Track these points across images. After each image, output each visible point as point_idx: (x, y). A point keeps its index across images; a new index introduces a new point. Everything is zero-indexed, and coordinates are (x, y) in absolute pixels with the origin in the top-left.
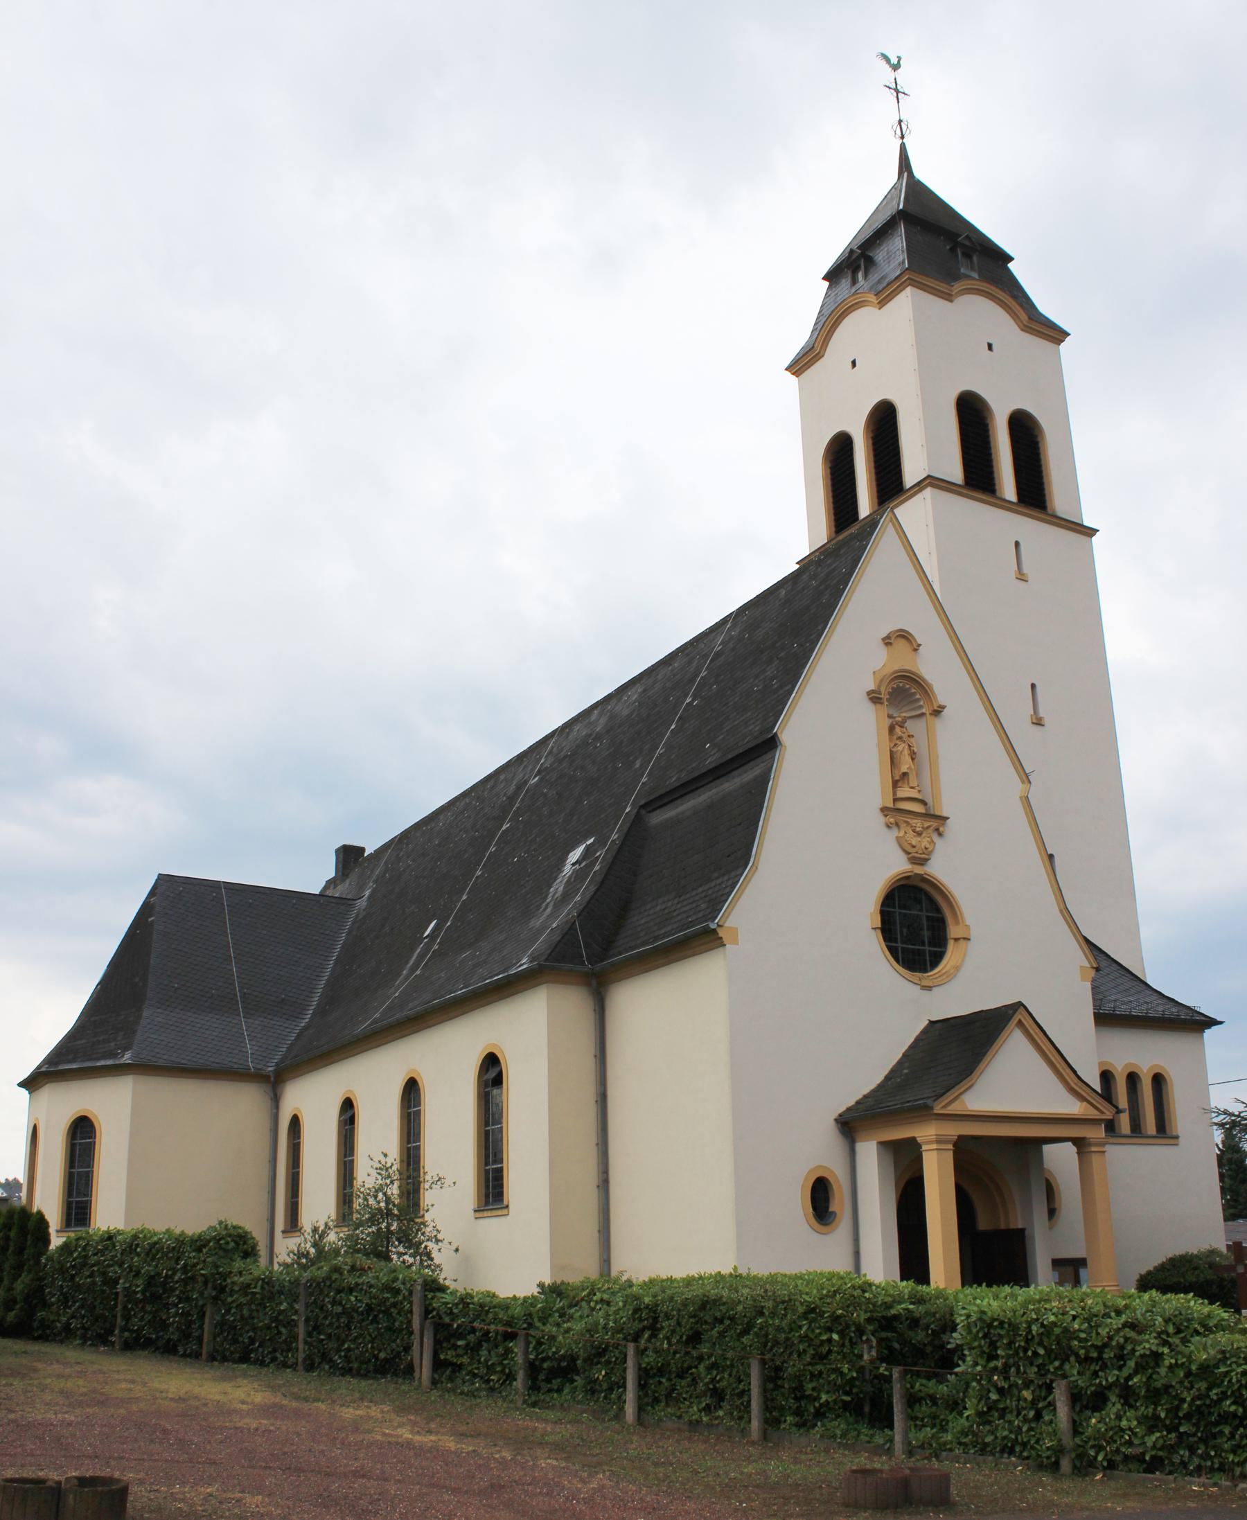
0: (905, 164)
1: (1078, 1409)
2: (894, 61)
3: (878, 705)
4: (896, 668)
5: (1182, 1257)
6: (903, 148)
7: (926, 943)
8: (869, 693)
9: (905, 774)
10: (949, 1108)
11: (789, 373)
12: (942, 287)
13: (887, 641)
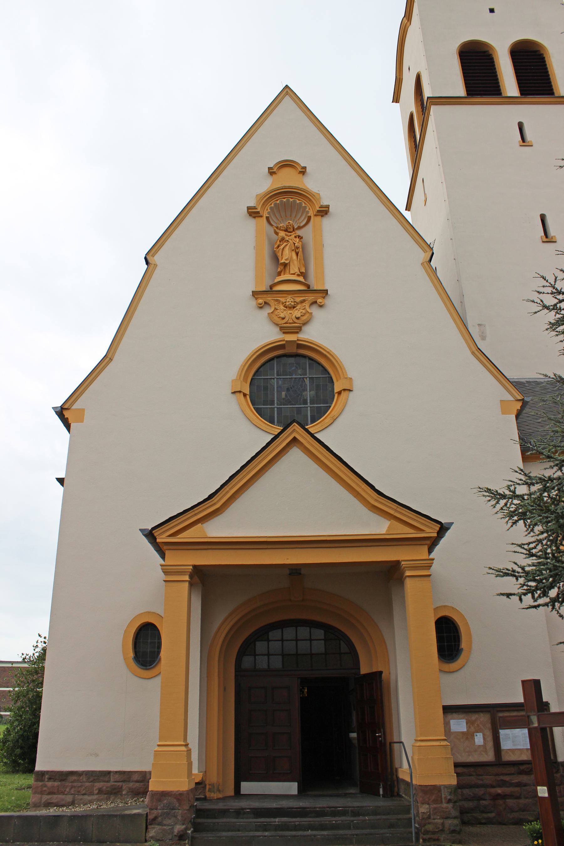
1: (530, 824)
7: (309, 401)
8: (249, 208)
10: (179, 536)
11: (407, 211)
13: (271, 172)
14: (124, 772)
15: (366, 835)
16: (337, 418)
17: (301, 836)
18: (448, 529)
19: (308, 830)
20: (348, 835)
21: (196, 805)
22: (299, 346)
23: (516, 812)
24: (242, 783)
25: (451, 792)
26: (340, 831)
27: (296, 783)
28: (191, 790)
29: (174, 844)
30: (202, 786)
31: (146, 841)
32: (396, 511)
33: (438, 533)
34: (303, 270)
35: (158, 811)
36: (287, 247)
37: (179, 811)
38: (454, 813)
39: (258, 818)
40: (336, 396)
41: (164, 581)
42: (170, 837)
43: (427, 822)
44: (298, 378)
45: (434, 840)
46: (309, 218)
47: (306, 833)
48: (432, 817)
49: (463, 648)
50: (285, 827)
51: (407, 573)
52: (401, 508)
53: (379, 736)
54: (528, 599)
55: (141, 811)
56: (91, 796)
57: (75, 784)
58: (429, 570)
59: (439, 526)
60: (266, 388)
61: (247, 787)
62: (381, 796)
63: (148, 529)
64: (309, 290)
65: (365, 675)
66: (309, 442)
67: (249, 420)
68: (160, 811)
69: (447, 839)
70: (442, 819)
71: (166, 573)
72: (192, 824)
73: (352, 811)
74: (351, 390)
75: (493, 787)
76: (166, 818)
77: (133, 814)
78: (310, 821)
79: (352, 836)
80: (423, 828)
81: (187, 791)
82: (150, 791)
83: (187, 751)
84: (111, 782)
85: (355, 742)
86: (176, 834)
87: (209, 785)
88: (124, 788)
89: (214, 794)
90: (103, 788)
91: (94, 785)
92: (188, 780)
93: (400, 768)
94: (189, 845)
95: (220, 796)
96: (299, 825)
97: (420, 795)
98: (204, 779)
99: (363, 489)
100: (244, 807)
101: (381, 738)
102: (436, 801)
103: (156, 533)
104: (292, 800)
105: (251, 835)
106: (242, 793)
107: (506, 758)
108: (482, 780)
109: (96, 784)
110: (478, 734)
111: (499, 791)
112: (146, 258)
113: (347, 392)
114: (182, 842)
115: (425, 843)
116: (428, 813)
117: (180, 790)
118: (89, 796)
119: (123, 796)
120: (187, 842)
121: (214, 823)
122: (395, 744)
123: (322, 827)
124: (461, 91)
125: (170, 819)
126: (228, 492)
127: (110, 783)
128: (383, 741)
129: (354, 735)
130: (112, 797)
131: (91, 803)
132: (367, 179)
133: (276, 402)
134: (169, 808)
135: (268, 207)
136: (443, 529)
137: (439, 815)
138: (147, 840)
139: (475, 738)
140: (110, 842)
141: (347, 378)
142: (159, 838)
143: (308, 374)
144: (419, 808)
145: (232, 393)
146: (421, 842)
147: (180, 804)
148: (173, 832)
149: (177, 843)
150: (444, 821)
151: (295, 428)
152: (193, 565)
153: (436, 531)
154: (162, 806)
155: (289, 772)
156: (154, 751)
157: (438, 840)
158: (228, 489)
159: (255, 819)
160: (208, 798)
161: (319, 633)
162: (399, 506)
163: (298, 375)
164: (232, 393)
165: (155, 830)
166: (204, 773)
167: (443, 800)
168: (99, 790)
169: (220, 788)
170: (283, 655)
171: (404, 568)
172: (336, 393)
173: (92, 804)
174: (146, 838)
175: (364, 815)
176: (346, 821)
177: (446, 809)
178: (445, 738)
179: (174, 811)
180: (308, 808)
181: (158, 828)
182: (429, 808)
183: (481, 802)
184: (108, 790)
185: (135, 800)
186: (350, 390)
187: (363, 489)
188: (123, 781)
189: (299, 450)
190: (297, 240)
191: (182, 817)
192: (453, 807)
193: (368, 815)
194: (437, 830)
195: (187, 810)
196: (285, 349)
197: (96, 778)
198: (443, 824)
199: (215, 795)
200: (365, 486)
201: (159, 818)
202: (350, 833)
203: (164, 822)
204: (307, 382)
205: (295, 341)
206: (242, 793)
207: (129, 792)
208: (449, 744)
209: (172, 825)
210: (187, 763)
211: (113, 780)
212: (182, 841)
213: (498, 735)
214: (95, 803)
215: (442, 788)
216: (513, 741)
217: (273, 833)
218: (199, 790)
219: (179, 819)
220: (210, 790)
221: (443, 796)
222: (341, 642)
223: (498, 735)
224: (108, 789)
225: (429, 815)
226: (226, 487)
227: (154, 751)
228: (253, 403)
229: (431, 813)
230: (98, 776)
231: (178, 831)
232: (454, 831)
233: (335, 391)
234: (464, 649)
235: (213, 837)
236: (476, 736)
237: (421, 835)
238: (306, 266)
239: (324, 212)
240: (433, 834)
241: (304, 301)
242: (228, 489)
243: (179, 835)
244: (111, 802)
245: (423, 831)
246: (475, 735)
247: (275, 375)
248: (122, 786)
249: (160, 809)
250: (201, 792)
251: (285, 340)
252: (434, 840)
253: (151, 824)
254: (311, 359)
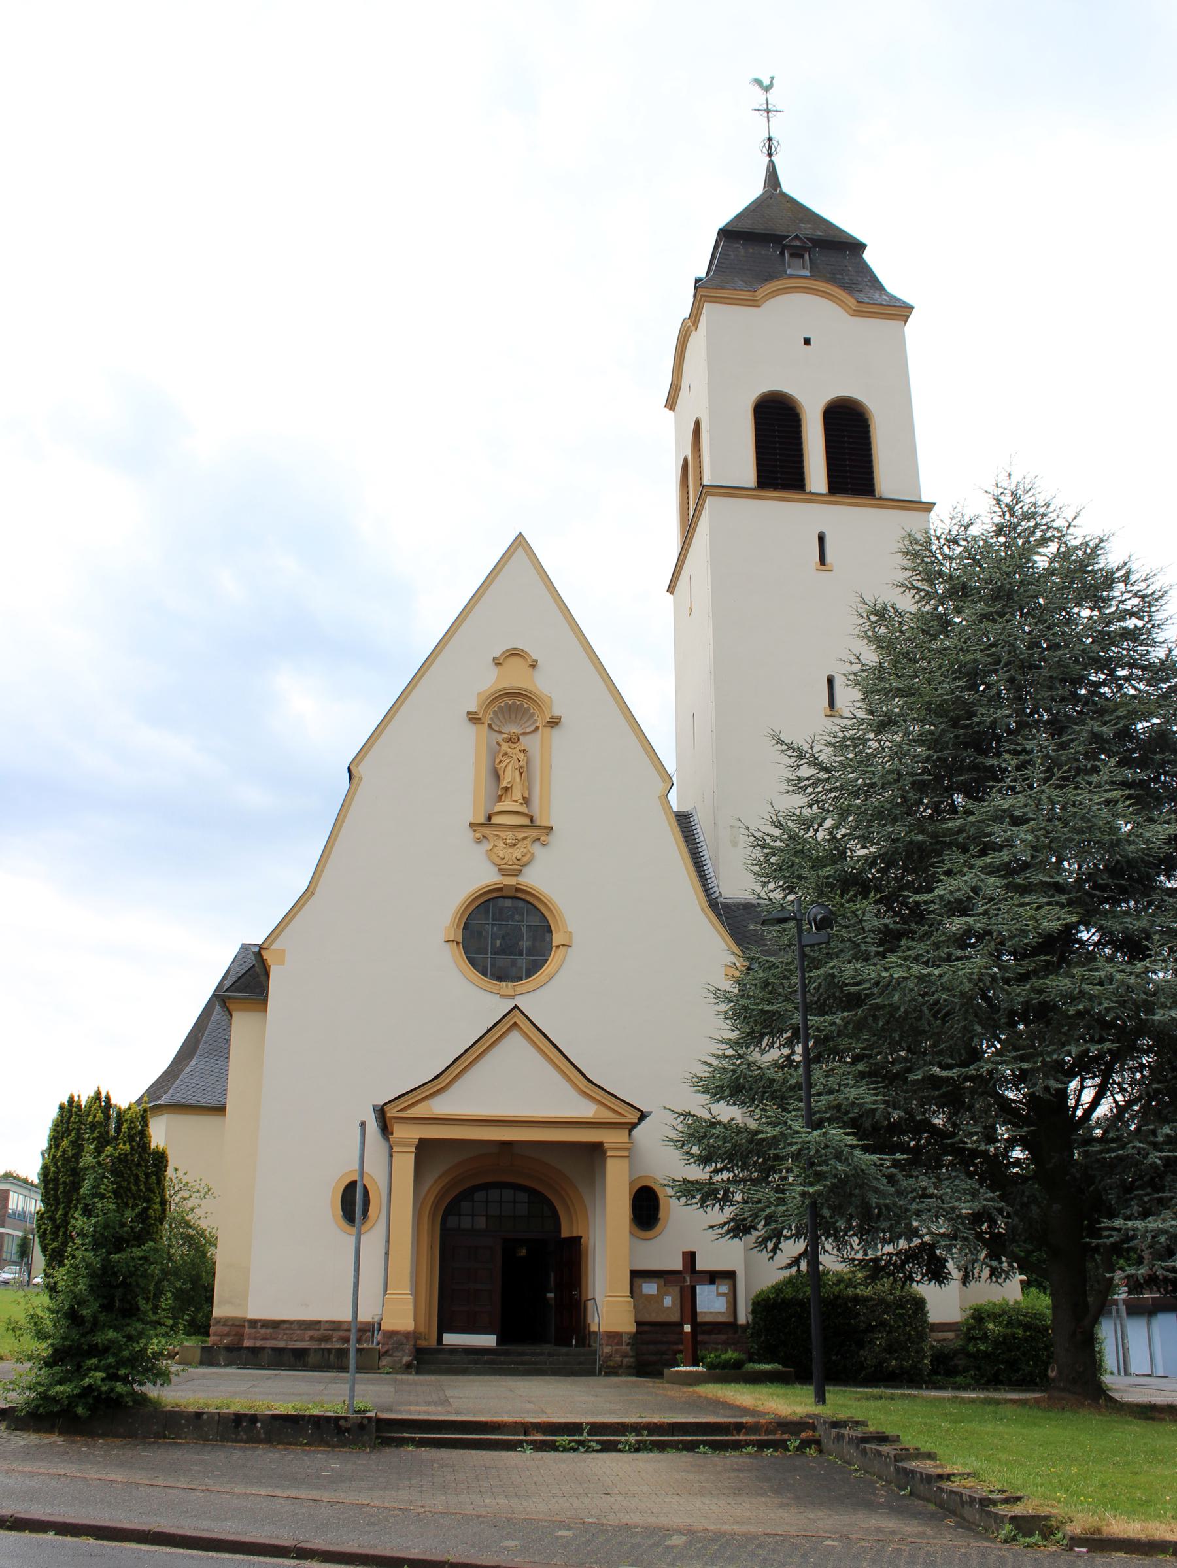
0: (772, 178)
2: (766, 82)
3: (477, 725)
4: (505, 685)
5: (56, 1139)
6: (772, 164)
8: (469, 713)
9: (507, 789)
12: (745, 295)
13: (497, 662)
22: (518, 890)
24: (563, 1236)
34: (526, 795)
36: (511, 764)
38: (631, 1354)
40: (554, 949)
46: (537, 728)
54: (683, 1199)
57: (288, 1332)
61: (450, 1339)
64: (532, 824)
85: (553, 1302)
102: (617, 1344)
103: (386, 1108)
112: (349, 769)
113: (566, 947)
124: (747, 475)
129: (551, 1295)
132: (607, 679)
135: (491, 710)
136: (643, 1116)
161: (523, 1197)
170: (487, 1216)
188: (334, 1330)
190: (522, 755)
198: (622, 1361)
204: (524, 929)
238: (530, 789)
239: (554, 723)
241: (526, 838)
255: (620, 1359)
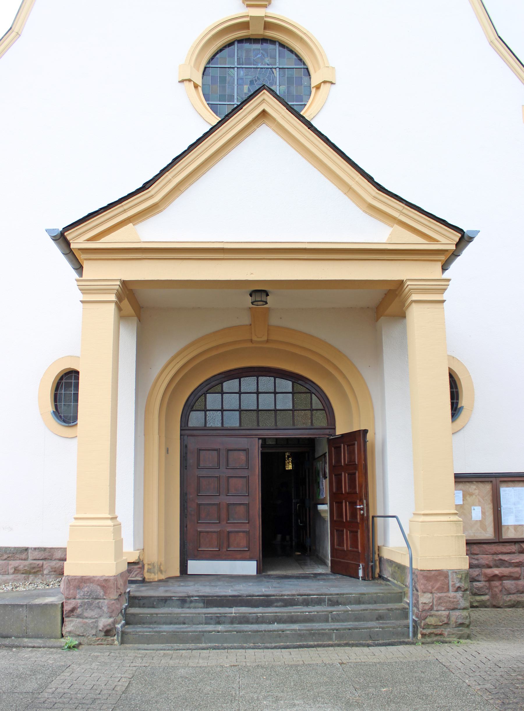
10: (103, 240)
14: (45, 549)
15: (350, 630)
16: (314, 117)
17: (265, 631)
18: (470, 239)
19: (274, 623)
20: (327, 631)
21: (129, 592)
22: (268, 26)
23: (514, 594)
24: (189, 562)
25: (461, 579)
26: (314, 624)
27: (255, 562)
28: (122, 574)
29: (100, 640)
30: (138, 566)
31: (62, 636)
32: (401, 213)
33: (457, 245)
35: (77, 600)
37: (105, 601)
39: (208, 608)
40: (313, 91)
41: (82, 302)
42: (94, 632)
43: (428, 614)
44: (265, 68)
45: (436, 635)
47: (271, 627)
48: (435, 608)
49: (463, 407)
50: (244, 620)
51: (413, 298)
52: (409, 208)
53: (361, 509)
55: (56, 600)
56: (6, 575)
58: (442, 295)
59: (460, 235)
60: (223, 80)
62: (361, 579)
63: (58, 229)
65: (343, 435)
66: (284, 116)
67: (201, 116)
68: (79, 601)
69: (453, 634)
70: (448, 610)
71: (84, 291)
72: (123, 616)
73: (329, 600)
74: (333, 82)
75: (490, 567)
76: (88, 610)
77: (44, 604)
78: (276, 613)
79: (332, 631)
80: (423, 622)
81: (115, 576)
82: (66, 576)
83: (114, 526)
84: (29, 560)
86: (101, 629)
87: (148, 564)
88: (45, 567)
89: (155, 575)
90: (20, 567)
91: (8, 564)
92: (115, 563)
93: (384, 546)
94: (118, 641)
95: (163, 577)
96: (263, 617)
97: (421, 582)
98: (141, 558)
99: (357, 183)
100: (191, 595)
101: (363, 510)
102: (441, 589)
103: (69, 235)
104: (251, 584)
105: (200, 630)
106: (189, 573)
107: (509, 534)
108: (477, 559)
109: (11, 562)
110: (476, 508)
111: (496, 571)
113: (328, 85)
114: (110, 639)
115: (425, 638)
116: (430, 603)
117: (105, 576)
118: (4, 575)
119: (45, 576)
120: (116, 637)
121: (152, 614)
122: (378, 518)
123: (292, 620)
125: (93, 610)
126: (170, 181)
127: (28, 561)
128: (365, 515)
130: (31, 577)
131: (6, 583)
133: (236, 97)
134: (91, 598)
137: (444, 606)
138: (64, 635)
139: (472, 512)
140: (15, 637)
141: (328, 67)
142: (79, 633)
143: (278, 64)
144: (419, 598)
145: (180, 82)
146: (419, 638)
147: (105, 593)
148: (97, 627)
149: (102, 639)
150: (449, 613)
151: (265, 97)
152: (121, 280)
153: (456, 243)
154: (82, 594)
155: (247, 549)
156: (70, 526)
157: (441, 634)
158: (170, 177)
159: (205, 609)
160: (147, 580)
161: (286, 385)
162: (406, 207)
163: (265, 65)
164: (180, 82)
165: (74, 623)
166: (142, 550)
167: (451, 588)
168: (15, 570)
169: (162, 568)
170: (240, 410)
171: (410, 289)
172: (313, 88)
173: (7, 585)
174: (63, 633)
175: (344, 604)
176: (323, 611)
177: (454, 598)
178: (456, 512)
179: (97, 601)
180: (274, 596)
181: (77, 622)
182: (432, 597)
183: (474, 583)
184: (26, 570)
185: (59, 581)
186: (332, 83)
187: (357, 183)
188: (45, 559)
189: (270, 129)
191: (108, 608)
192: (463, 597)
193: (350, 603)
194: (441, 624)
195: (115, 600)
196: (249, 30)
197: (10, 555)
198: (448, 617)
199: (156, 577)
200: (360, 177)
201: (78, 609)
202: (329, 627)
203: (86, 614)
204: (277, 73)
205: (262, 18)
206: (189, 573)
207: (51, 572)
208: (461, 519)
209: (97, 618)
210: (114, 541)
211: (31, 558)
212: (109, 637)
213: (499, 509)
214: (11, 583)
215: (450, 574)
216: (516, 517)
217: (228, 627)
218: (135, 571)
219: (105, 610)
220: (149, 571)
221: (451, 583)
222: (313, 395)
223: (499, 509)
224: (25, 568)
225: (431, 606)
226: (167, 173)
227: (70, 526)
228: (207, 97)
229: (435, 603)
230: (13, 554)
231: (103, 626)
232: (462, 625)
233: (312, 86)
234: (464, 407)
235: (150, 632)
236: (474, 509)
237: (420, 630)
240: (435, 628)
242: (170, 177)
243: (105, 630)
244: (30, 582)
245: (422, 625)
246: (472, 509)
247: (236, 63)
248: (43, 564)
249: (79, 599)
250: (137, 574)
251: (250, 15)
252: (436, 635)
253: (68, 617)
254: (282, 45)
255: (447, 613)
